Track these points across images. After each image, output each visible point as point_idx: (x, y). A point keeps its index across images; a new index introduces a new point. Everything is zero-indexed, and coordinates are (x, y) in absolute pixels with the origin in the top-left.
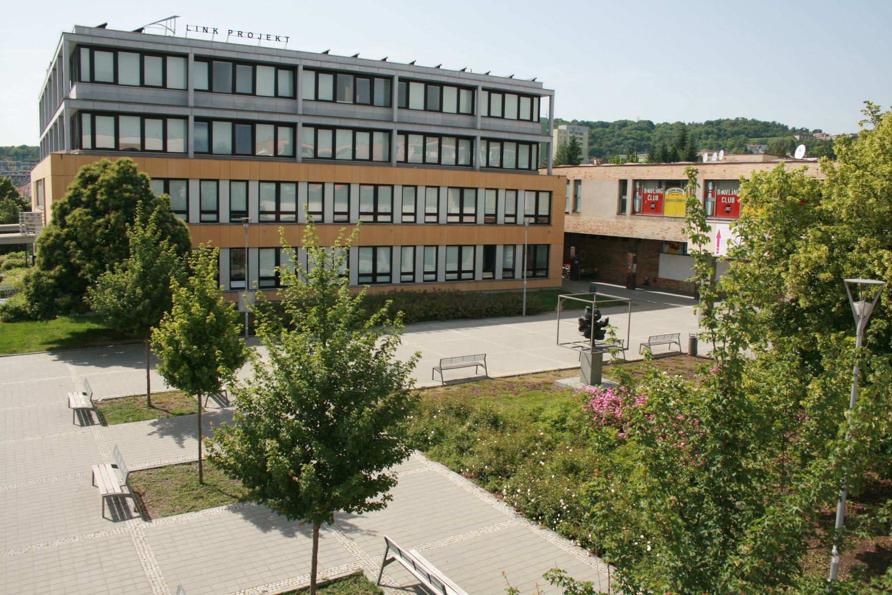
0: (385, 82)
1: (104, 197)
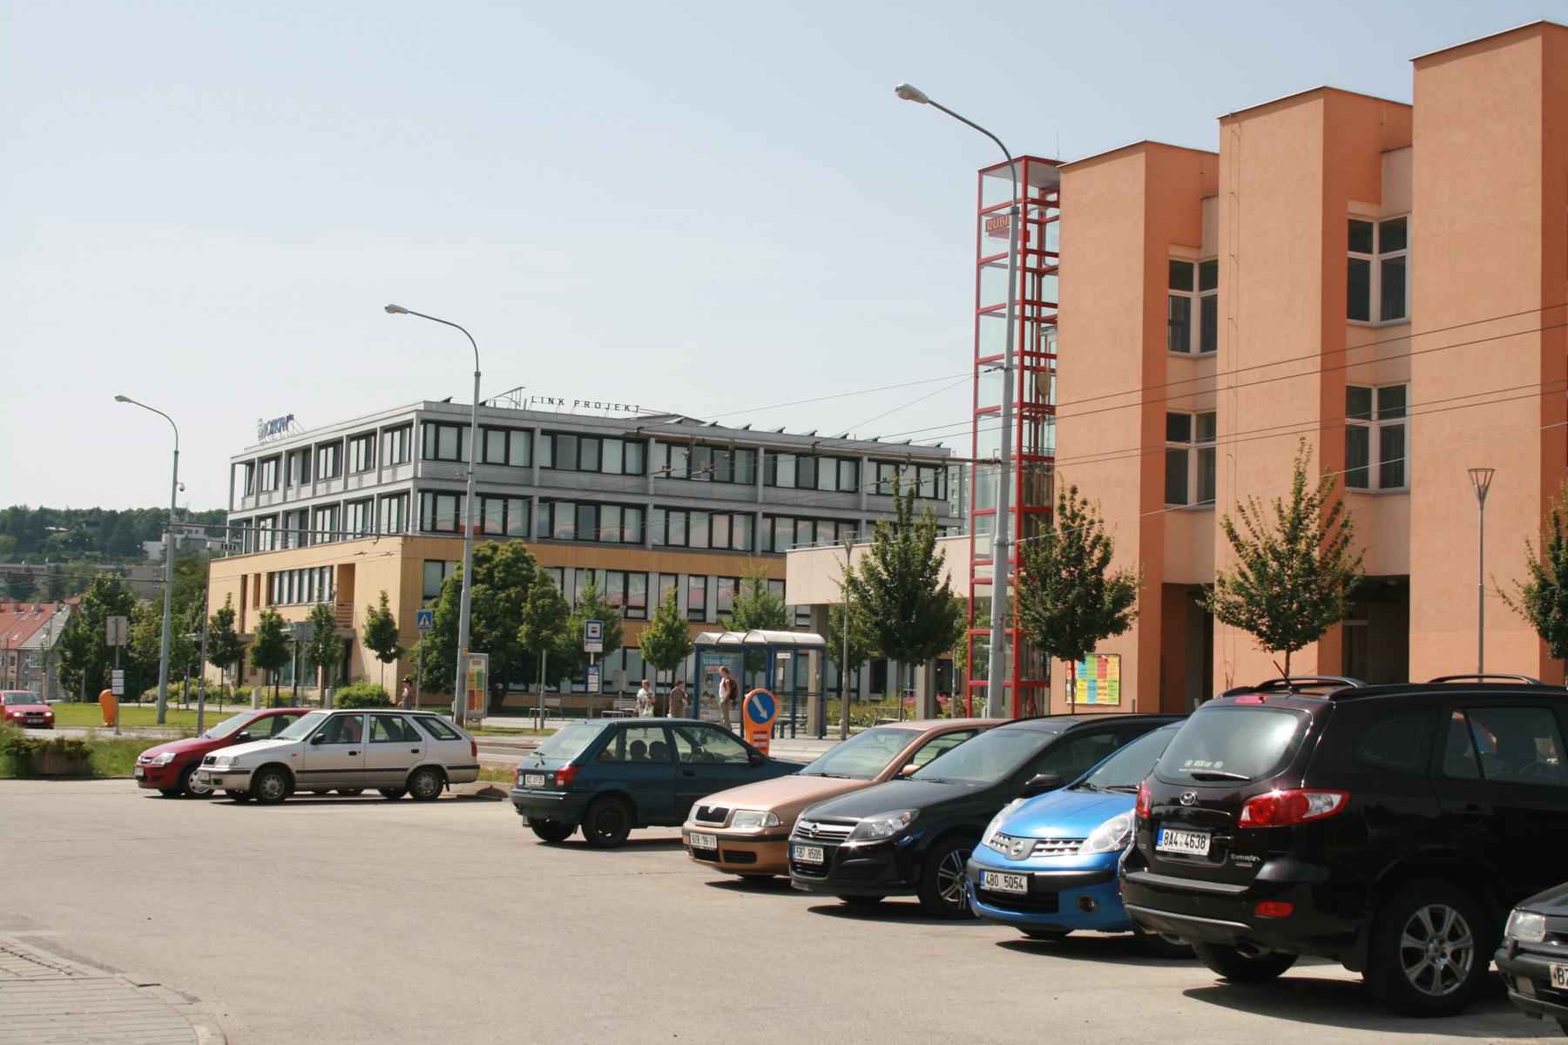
0: (748, 456)
1: (502, 575)
